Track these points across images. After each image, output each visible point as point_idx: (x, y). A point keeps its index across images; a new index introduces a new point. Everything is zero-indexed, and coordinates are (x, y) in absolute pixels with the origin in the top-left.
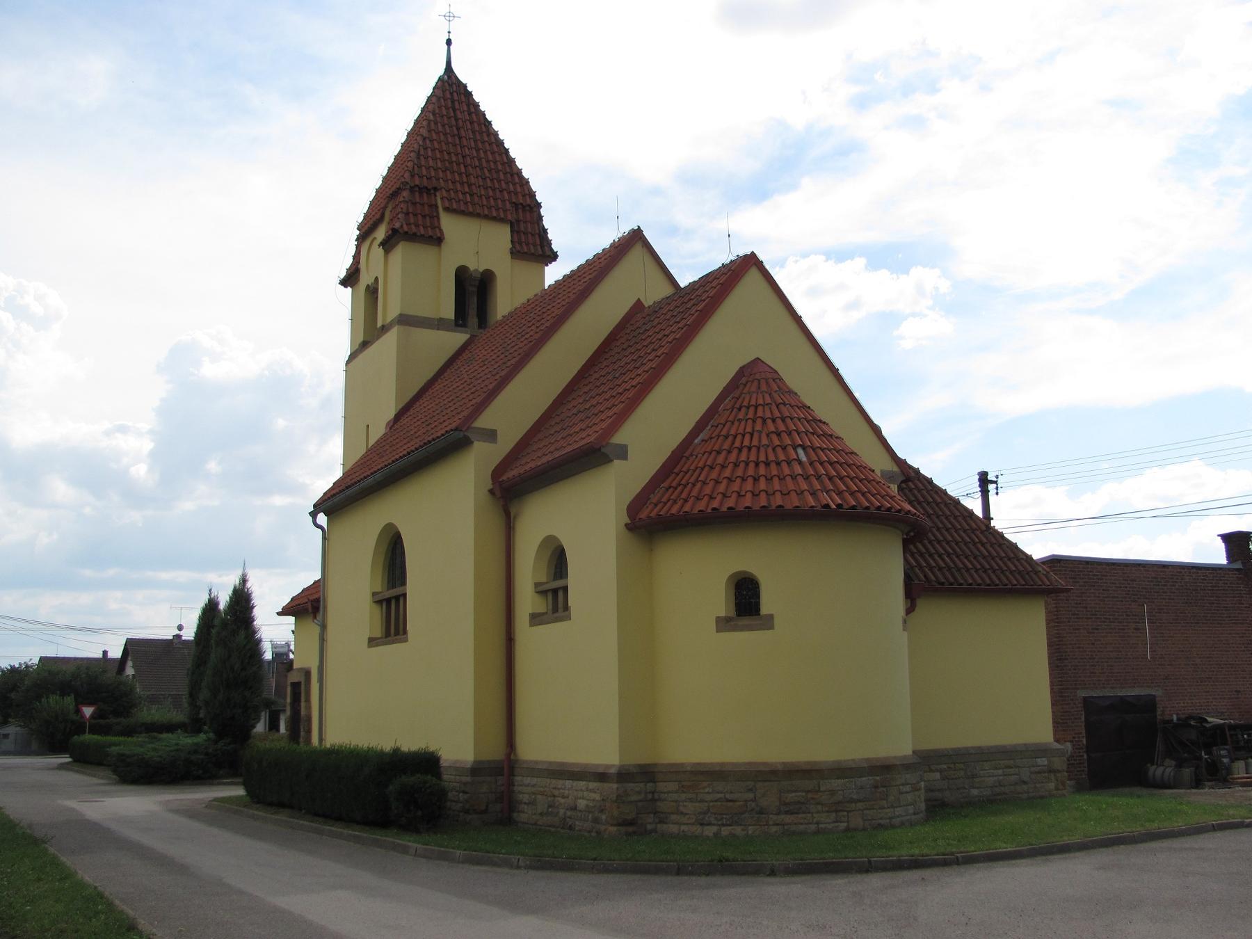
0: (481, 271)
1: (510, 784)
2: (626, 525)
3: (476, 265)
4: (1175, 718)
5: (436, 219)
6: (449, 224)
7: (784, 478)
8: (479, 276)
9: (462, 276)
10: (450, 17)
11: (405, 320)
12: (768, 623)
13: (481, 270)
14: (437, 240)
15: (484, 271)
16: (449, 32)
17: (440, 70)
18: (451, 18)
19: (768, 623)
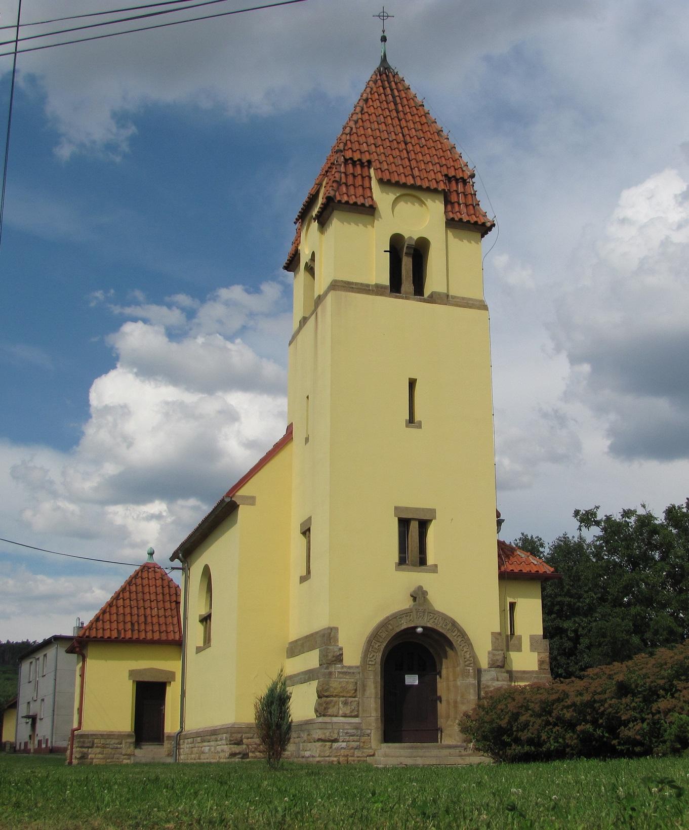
0: (415, 239)
1: (639, 650)
2: (674, 507)
3: (411, 232)
4: (602, 757)
5: (368, 190)
6: (382, 198)
7: (381, 95)
8: (414, 243)
9: (396, 247)
10: (383, 16)
11: (335, 286)
12: (419, 426)
13: (415, 238)
14: (369, 211)
15: (418, 239)
16: (384, 31)
17: (377, 63)
18: (382, 14)
19: (419, 426)
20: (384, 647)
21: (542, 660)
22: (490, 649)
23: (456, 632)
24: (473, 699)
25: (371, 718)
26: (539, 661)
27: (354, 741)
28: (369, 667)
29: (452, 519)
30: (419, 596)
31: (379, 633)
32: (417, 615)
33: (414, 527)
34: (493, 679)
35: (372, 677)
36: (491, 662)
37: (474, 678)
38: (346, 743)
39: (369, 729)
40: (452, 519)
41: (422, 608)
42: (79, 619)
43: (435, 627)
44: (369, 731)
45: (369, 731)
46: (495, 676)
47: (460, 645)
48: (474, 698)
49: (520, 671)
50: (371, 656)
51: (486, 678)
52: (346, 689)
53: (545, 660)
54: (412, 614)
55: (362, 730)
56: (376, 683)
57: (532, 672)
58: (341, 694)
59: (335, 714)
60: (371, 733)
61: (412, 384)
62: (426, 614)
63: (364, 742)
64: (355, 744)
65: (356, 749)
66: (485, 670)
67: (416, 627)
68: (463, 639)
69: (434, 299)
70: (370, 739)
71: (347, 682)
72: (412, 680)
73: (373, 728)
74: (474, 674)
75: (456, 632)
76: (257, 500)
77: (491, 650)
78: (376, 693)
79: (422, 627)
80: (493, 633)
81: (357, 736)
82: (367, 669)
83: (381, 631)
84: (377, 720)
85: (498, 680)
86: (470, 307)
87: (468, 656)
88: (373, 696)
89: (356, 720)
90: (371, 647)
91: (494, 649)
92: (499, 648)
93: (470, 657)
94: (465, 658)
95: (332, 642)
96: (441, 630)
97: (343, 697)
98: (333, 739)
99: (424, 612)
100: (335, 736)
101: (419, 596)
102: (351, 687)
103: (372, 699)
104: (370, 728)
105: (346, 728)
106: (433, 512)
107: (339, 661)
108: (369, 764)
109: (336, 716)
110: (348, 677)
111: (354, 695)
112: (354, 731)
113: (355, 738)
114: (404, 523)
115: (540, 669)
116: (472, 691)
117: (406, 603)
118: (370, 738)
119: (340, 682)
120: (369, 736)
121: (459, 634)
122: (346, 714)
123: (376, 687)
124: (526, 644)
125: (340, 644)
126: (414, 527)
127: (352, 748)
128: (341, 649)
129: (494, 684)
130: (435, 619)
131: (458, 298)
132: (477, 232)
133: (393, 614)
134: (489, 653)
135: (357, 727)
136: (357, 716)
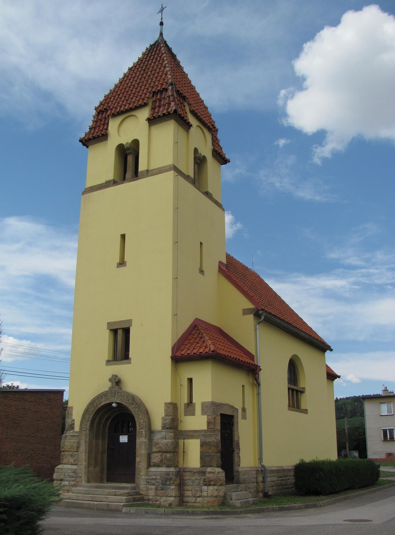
20: (91, 418)
21: (209, 421)
22: (163, 415)
23: (135, 405)
24: (144, 453)
25: (82, 466)
26: (207, 422)
27: (72, 481)
28: (83, 432)
29: (142, 324)
30: (117, 382)
31: (88, 409)
32: (111, 395)
33: (120, 333)
34: (162, 438)
35: (84, 439)
36: (163, 425)
37: (146, 437)
38: (68, 482)
39: (81, 473)
40: (142, 324)
41: (114, 390)
42: (384, 386)
43: (122, 402)
44: (81, 475)
45: (81, 475)
46: (164, 435)
47: (137, 414)
48: (144, 452)
49: (193, 431)
50: (84, 424)
51: (157, 438)
52: (73, 446)
53: (211, 421)
54: (108, 394)
55: (77, 473)
56: (85, 442)
57: (202, 431)
58: (70, 450)
59: (67, 463)
60: (82, 476)
61: (123, 237)
62: (117, 393)
63: (78, 482)
64: (73, 483)
65: (73, 486)
66: (158, 432)
67: (113, 403)
68: (139, 409)
69: (148, 173)
70: (82, 480)
71: (74, 442)
72: (124, 439)
73: (83, 472)
74: (146, 435)
75: (135, 405)
76: (109, 322)
77: (164, 416)
78: (86, 449)
79: (117, 403)
80: (165, 403)
81: (74, 477)
82: (82, 433)
83: (90, 408)
84: (85, 467)
85: (166, 439)
86: (161, 173)
87: (142, 422)
88: (84, 451)
89: (75, 467)
90: (84, 418)
91: (166, 415)
92: (170, 414)
93: (143, 422)
94: (140, 423)
95: (69, 416)
96: (125, 404)
97: (71, 451)
98: (60, 479)
99: (115, 393)
100: (62, 477)
101: (117, 382)
102: (75, 445)
103: (84, 453)
104: (81, 472)
105: (69, 472)
106: (130, 321)
107: (72, 429)
108: (5, 498)
109: (67, 464)
110: (75, 439)
111: (77, 450)
112: (72, 474)
113: (73, 479)
114: (115, 332)
115: (208, 428)
116: (143, 447)
117: (106, 386)
118: (81, 479)
119: (70, 442)
120: (80, 478)
121: (136, 406)
122: (71, 463)
123: (86, 446)
124: (198, 409)
125: (74, 418)
126: (120, 333)
127: (71, 486)
128: (74, 420)
129: (162, 442)
130: (122, 397)
131: (155, 169)
132: (171, 120)
133: (97, 396)
134: (162, 418)
135: (75, 472)
136: (76, 464)
